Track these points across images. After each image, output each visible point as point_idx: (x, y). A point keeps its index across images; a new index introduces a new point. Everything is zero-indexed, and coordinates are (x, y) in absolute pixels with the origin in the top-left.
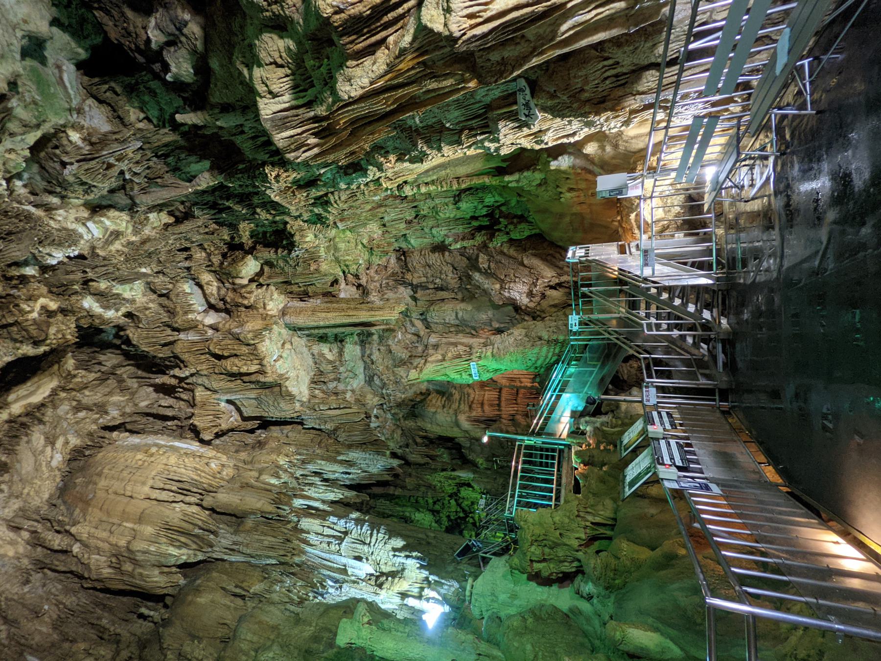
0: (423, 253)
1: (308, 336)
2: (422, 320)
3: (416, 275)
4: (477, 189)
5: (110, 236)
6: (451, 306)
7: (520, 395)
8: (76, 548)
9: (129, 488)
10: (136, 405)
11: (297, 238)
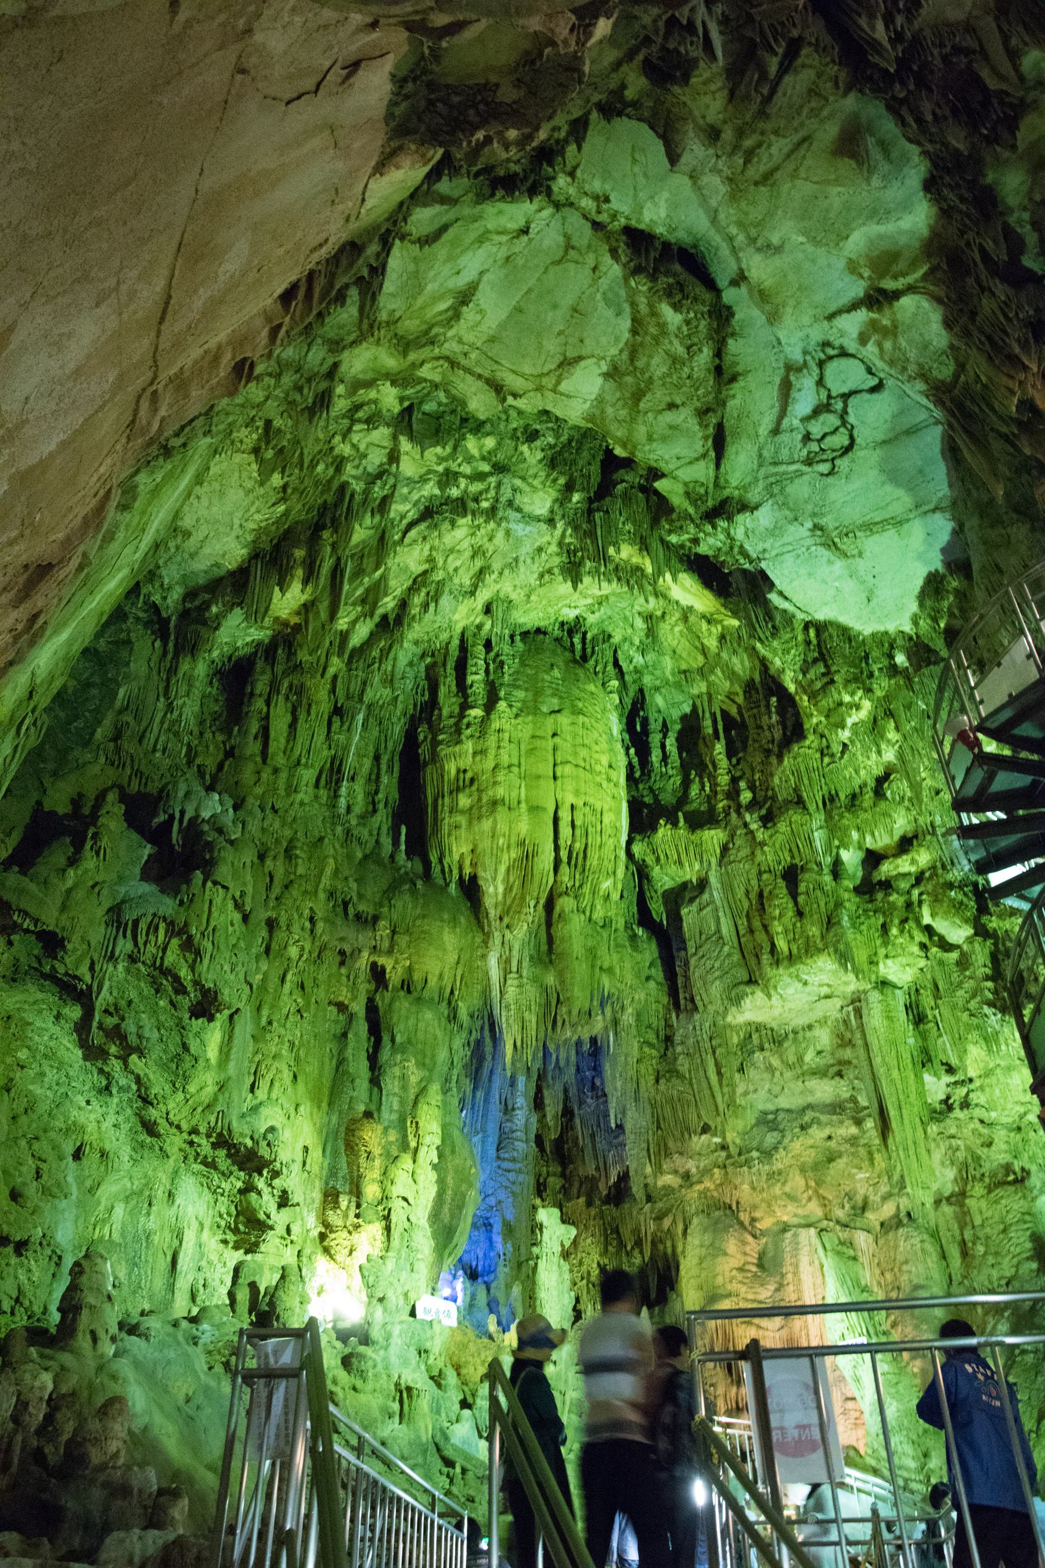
0: (1027, 1218)
1: (846, 1022)
2: (897, 1215)
3: (983, 1204)
6: (936, 1275)
8: (477, 713)
9: (568, 769)
10: (657, 689)
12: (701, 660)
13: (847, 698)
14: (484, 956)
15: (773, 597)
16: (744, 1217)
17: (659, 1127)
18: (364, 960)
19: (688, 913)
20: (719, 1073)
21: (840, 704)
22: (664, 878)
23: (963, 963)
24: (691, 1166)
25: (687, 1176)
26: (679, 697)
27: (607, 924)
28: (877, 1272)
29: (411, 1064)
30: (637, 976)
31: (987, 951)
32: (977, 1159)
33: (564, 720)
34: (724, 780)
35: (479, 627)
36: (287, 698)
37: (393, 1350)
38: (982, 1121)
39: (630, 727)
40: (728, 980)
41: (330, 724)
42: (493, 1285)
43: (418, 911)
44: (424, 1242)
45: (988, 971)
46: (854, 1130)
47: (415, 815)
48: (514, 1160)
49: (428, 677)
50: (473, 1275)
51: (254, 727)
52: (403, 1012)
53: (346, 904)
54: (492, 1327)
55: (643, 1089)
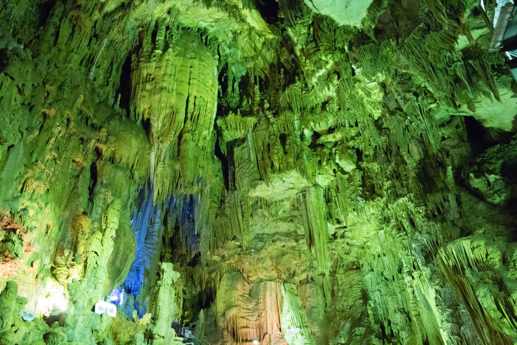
0: (360, 283)
2: (307, 278)
3: (343, 276)
4: (410, 326)
5: (368, 91)
8: (159, 52)
9: (195, 81)
10: (233, 64)
11: (372, 202)
12: (253, 53)
13: (324, 58)
16: (245, 275)
17: (215, 236)
18: (92, 144)
19: (237, 151)
20: (243, 216)
21: (321, 60)
22: (228, 136)
23: (350, 179)
24: (226, 253)
25: (223, 257)
26: (241, 68)
27: (204, 149)
29: (109, 194)
30: (214, 172)
31: (360, 176)
32: (342, 259)
33: (196, 62)
34: (258, 99)
35: (165, 19)
36: (70, 21)
37: (78, 330)
38: (348, 244)
39: (220, 79)
40: (252, 177)
41: (90, 40)
42: (137, 296)
43: (122, 128)
44: (103, 276)
45: (360, 183)
46: (294, 244)
47: (126, 92)
48: (152, 244)
49: (139, 36)
50: (129, 291)
51: (52, 30)
53: (87, 119)
54: (135, 315)
55: (210, 219)
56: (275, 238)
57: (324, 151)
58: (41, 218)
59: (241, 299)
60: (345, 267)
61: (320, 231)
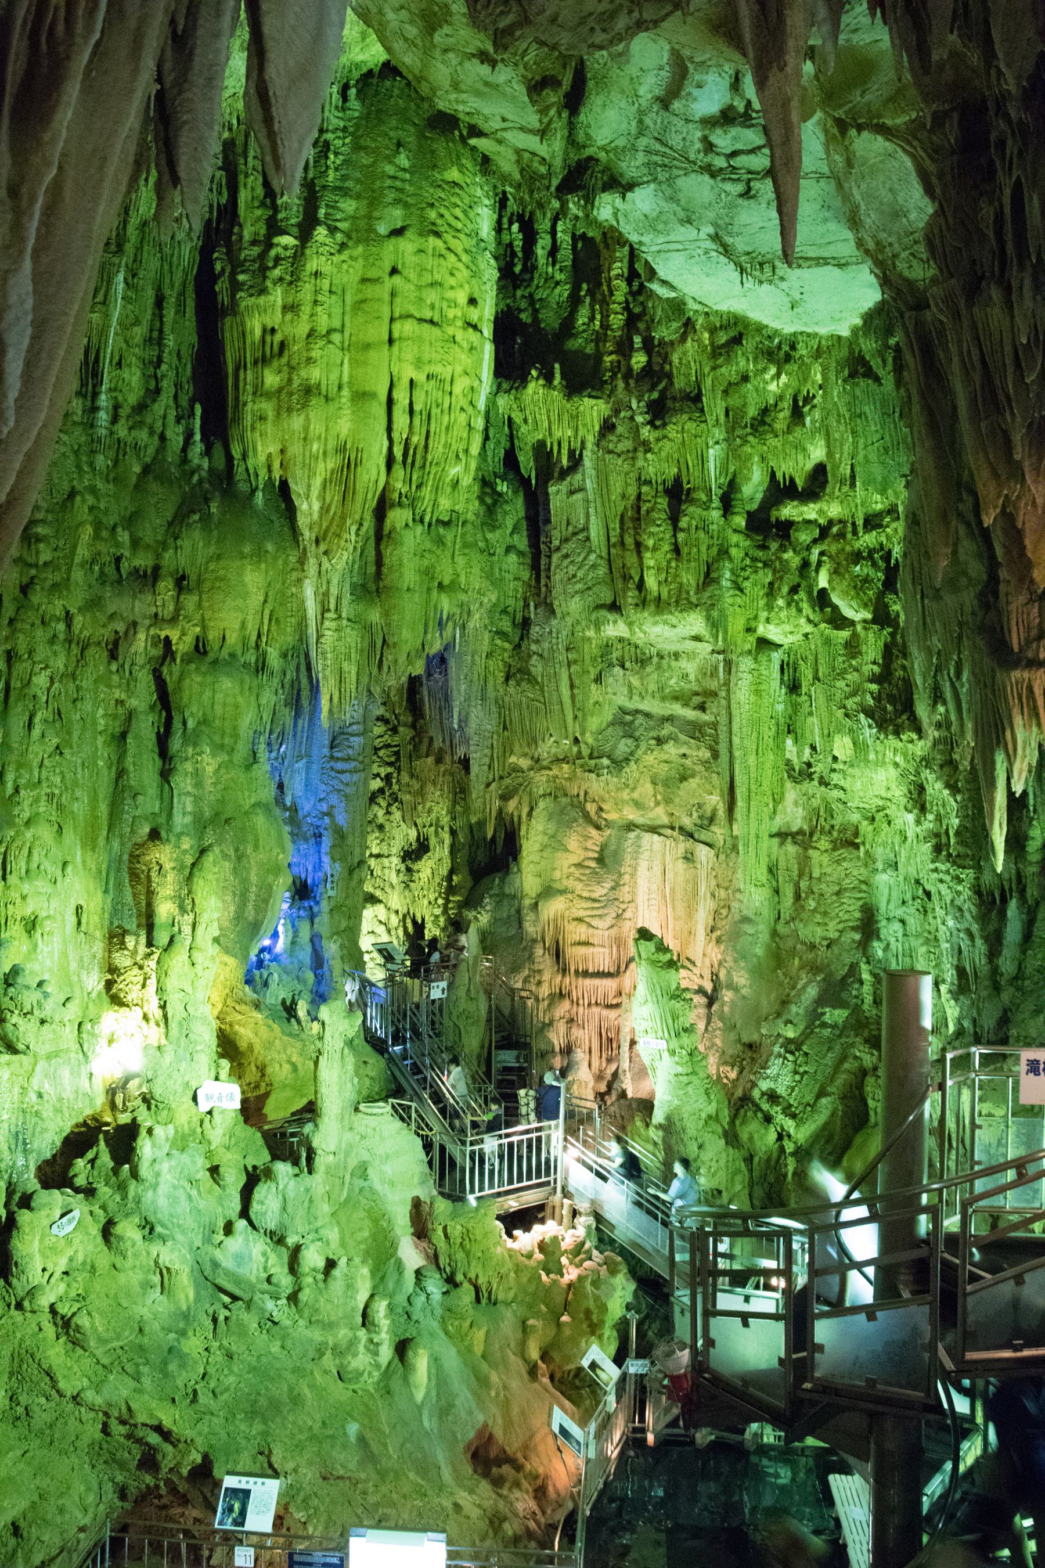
0: (864, 887)
3: (825, 859)
6: (765, 912)
7: (605, 1012)
14: (299, 581)
15: (655, 286)
17: (505, 728)
23: (852, 647)
28: (714, 883)
43: (212, 549)
47: (214, 394)
52: (196, 688)
56: (664, 732)
57: (786, 556)
58: (62, 894)
59: (577, 873)
60: (835, 834)
61: (753, 787)
